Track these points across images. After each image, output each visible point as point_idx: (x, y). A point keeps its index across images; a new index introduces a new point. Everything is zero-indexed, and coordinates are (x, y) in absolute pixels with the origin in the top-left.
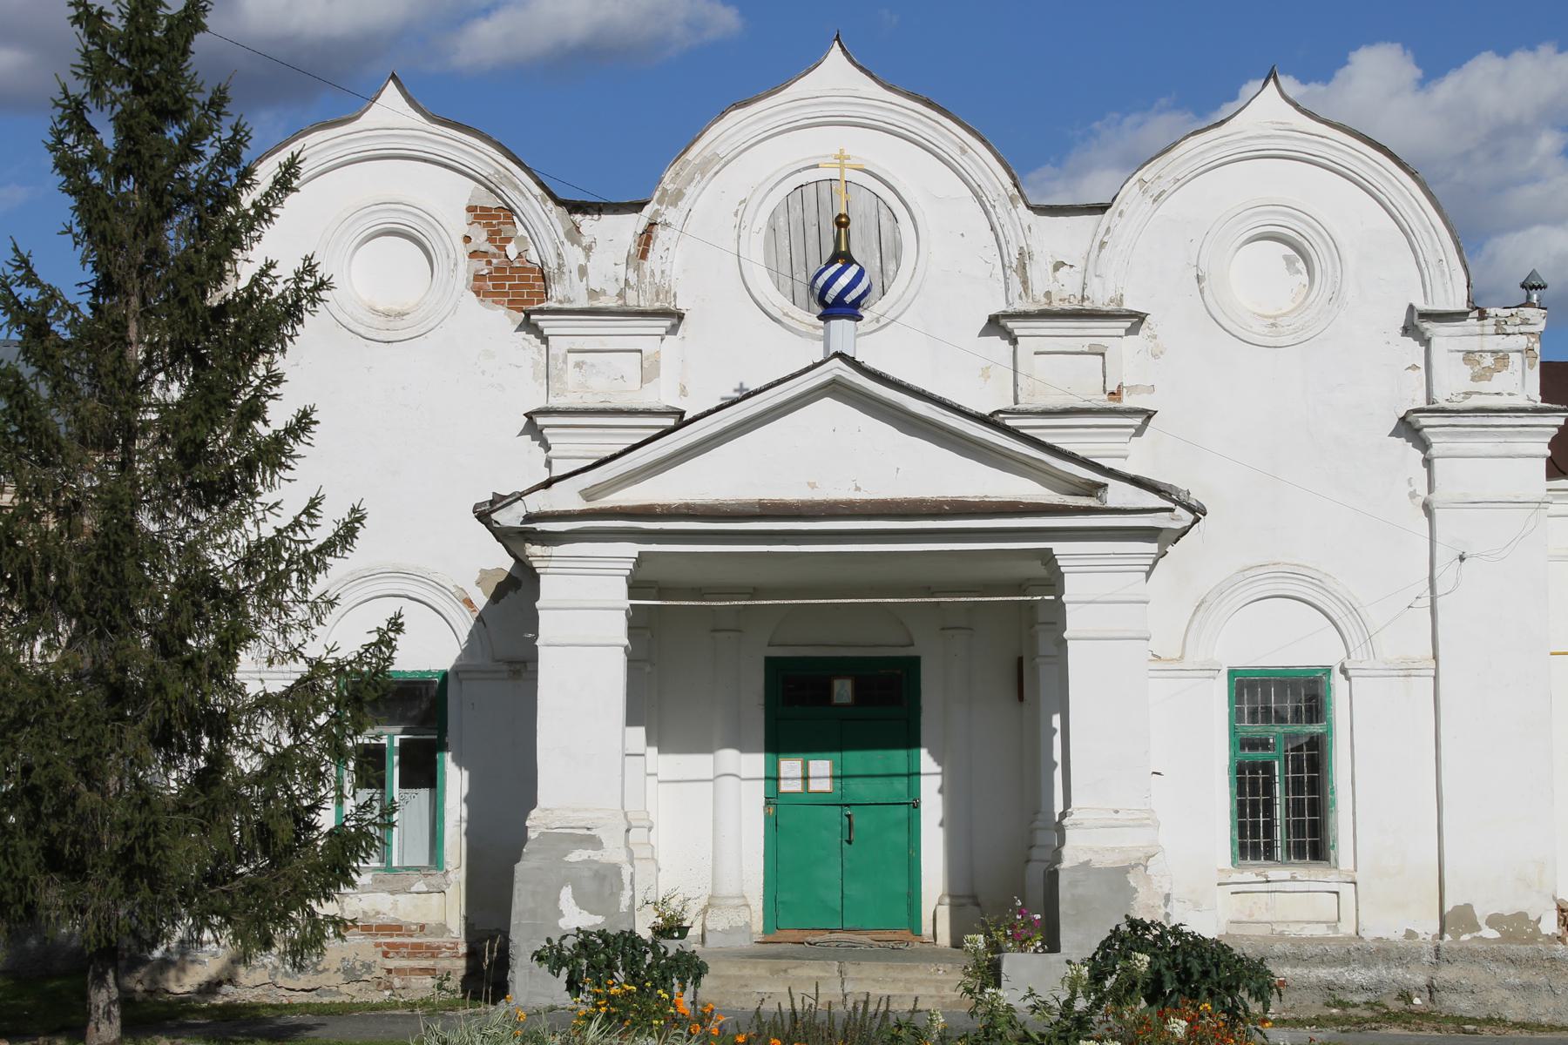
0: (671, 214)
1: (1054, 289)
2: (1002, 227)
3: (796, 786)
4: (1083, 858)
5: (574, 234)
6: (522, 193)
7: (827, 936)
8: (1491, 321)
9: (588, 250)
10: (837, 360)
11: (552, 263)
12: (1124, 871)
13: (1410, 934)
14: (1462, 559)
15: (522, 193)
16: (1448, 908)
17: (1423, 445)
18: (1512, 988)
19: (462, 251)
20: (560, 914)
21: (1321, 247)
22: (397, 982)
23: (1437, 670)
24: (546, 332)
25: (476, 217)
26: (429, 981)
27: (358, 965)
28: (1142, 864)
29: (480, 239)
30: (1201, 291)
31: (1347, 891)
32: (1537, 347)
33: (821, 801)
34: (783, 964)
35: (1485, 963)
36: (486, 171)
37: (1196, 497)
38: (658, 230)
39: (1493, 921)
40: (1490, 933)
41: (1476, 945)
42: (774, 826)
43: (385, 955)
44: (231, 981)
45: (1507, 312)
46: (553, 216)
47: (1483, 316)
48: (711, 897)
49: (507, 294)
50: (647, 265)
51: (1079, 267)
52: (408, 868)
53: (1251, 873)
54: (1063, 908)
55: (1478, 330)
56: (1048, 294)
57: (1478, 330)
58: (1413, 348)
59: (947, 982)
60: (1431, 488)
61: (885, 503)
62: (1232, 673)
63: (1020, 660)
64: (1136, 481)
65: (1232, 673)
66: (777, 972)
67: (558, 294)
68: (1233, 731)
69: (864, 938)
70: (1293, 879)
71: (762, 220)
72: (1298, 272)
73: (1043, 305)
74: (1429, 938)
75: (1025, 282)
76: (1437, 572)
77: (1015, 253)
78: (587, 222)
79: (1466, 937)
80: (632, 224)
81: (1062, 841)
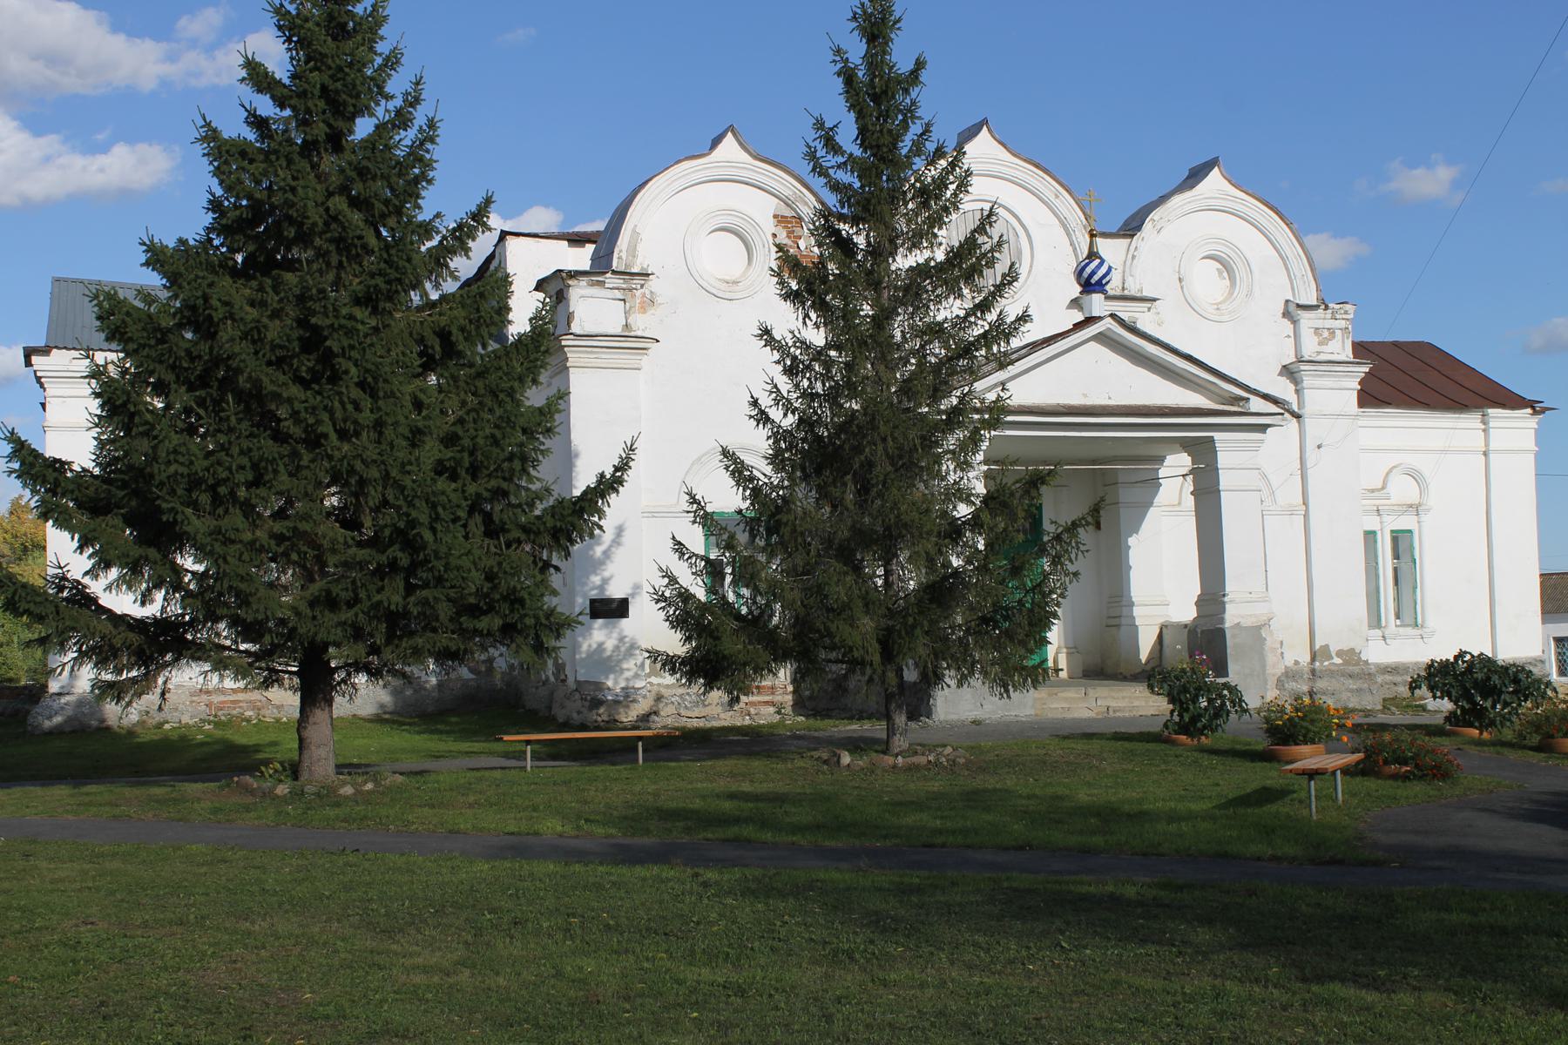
12: (1259, 628)
13: (1297, 663)
14: (1319, 447)
18: (1352, 691)
21: (1240, 264)
22: (752, 711)
23: (1307, 511)
26: (772, 710)
28: (1267, 624)
39: (1340, 653)
40: (1338, 661)
44: (655, 713)
47: (1327, 308)
58: (1287, 326)
61: (1138, 407)
64: (1266, 397)
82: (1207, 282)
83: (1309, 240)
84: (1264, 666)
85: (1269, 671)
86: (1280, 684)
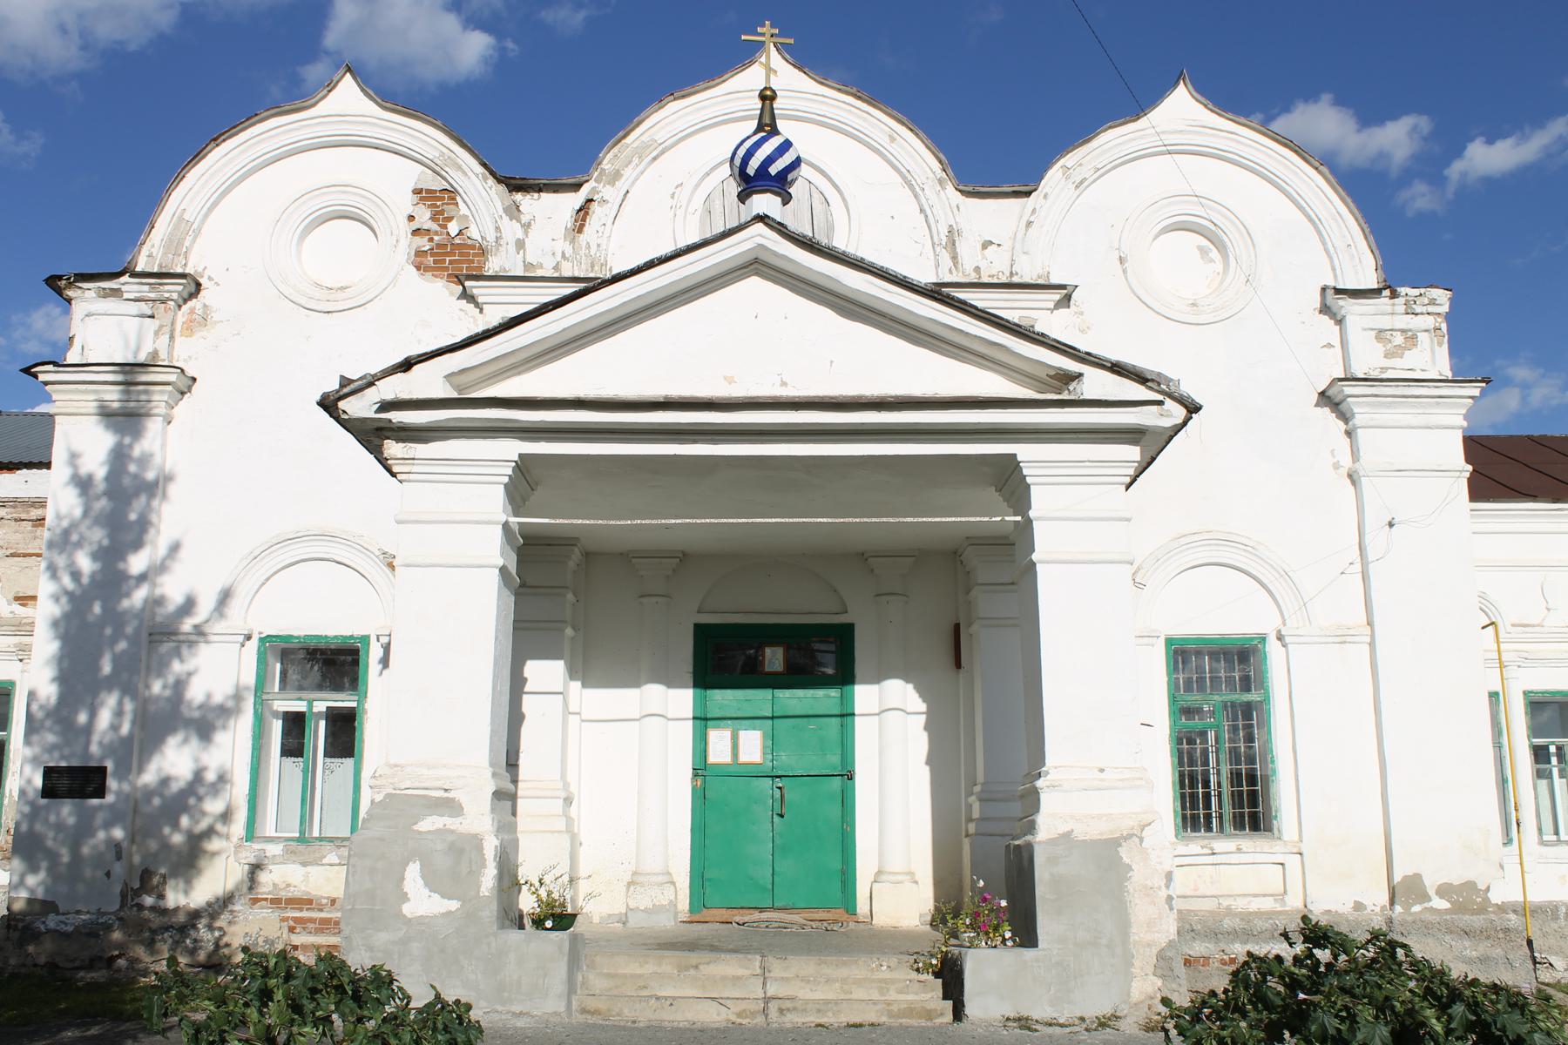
0: (607, 192)
1: (983, 265)
2: (931, 207)
3: (726, 758)
4: (1063, 829)
5: (514, 211)
6: (465, 173)
7: (757, 915)
8: (1401, 300)
9: (527, 227)
10: (760, 226)
11: (491, 237)
12: (1114, 843)
13: (1358, 906)
14: (1391, 525)
15: (465, 173)
16: (1397, 878)
17: (1345, 417)
19: (405, 228)
20: (404, 898)
23: (1373, 636)
24: (480, 300)
25: (421, 199)
27: (260, 940)
29: (424, 218)
30: (1125, 271)
31: (1293, 862)
32: (1444, 326)
33: (753, 773)
34: (694, 958)
35: (1440, 935)
36: (431, 154)
37: (1188, 388)
38: (594, 206)
39: (1443, 891)
40: (1441, 904)
41: (1428, 917)
42: (701, 798)
43: (292, 930)
45: (1416, 292)
46: (493, 193)
48: (635, 873)
49: (446, 269)
50: (583, 238)
51: (1007, 245)
52: (331, 840)
53: (1196, 845)
54: (1041, 891)
55: (1389, 309)
56: (977, 269)
57: (1389, 309)
59: (893, 981)
60: (1355, 456)
62: (1169, 641)
63: (957, 628)
64: (1117, 369)
65: (1169, 641)
66: (687, 968)
67: (493, 266)
68: (1173, 699)
69: (797, 918)
70: (1239, 850)
71: (698, 201)
72: (1212, 261)
73: (973, 278)
74: (1377, 909)
75: (954, 258)
76: (1367, 539)
77: (944, 231)
78: (526, 201)
79: (1416, 908)
80: (569, 202)
81: (1035, 806)
82: (1178, 267)
83: (1277, 126)
84: (1124, 925)
85: (1138, 933)
86: (1163, 964)
